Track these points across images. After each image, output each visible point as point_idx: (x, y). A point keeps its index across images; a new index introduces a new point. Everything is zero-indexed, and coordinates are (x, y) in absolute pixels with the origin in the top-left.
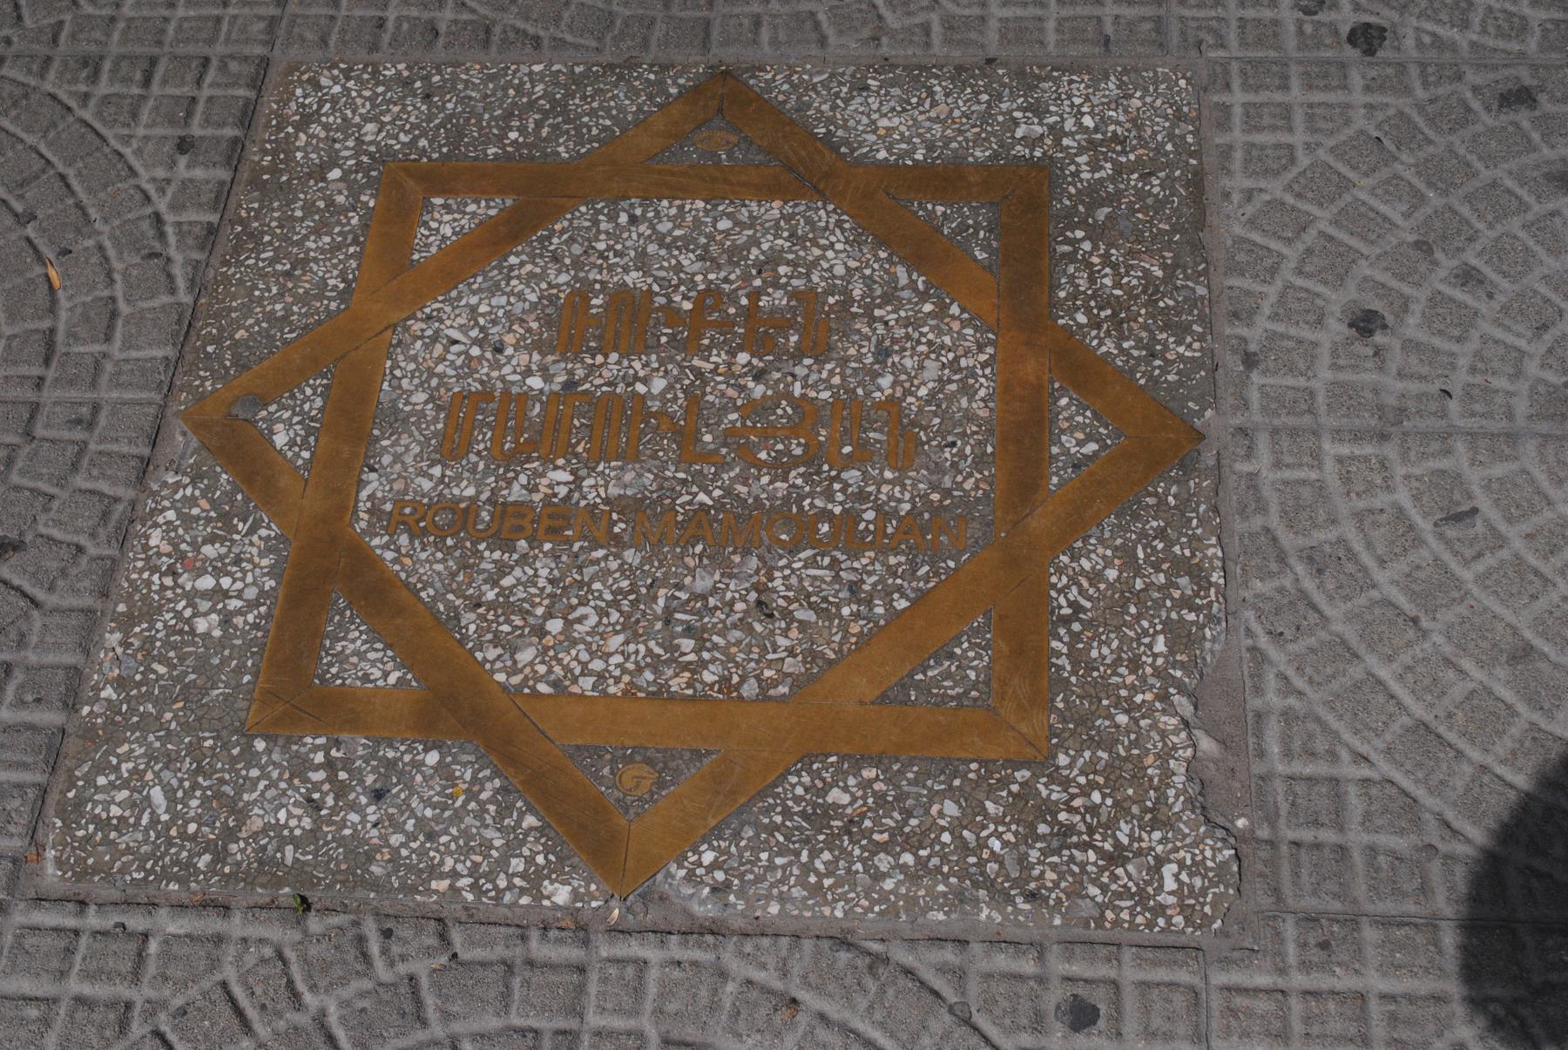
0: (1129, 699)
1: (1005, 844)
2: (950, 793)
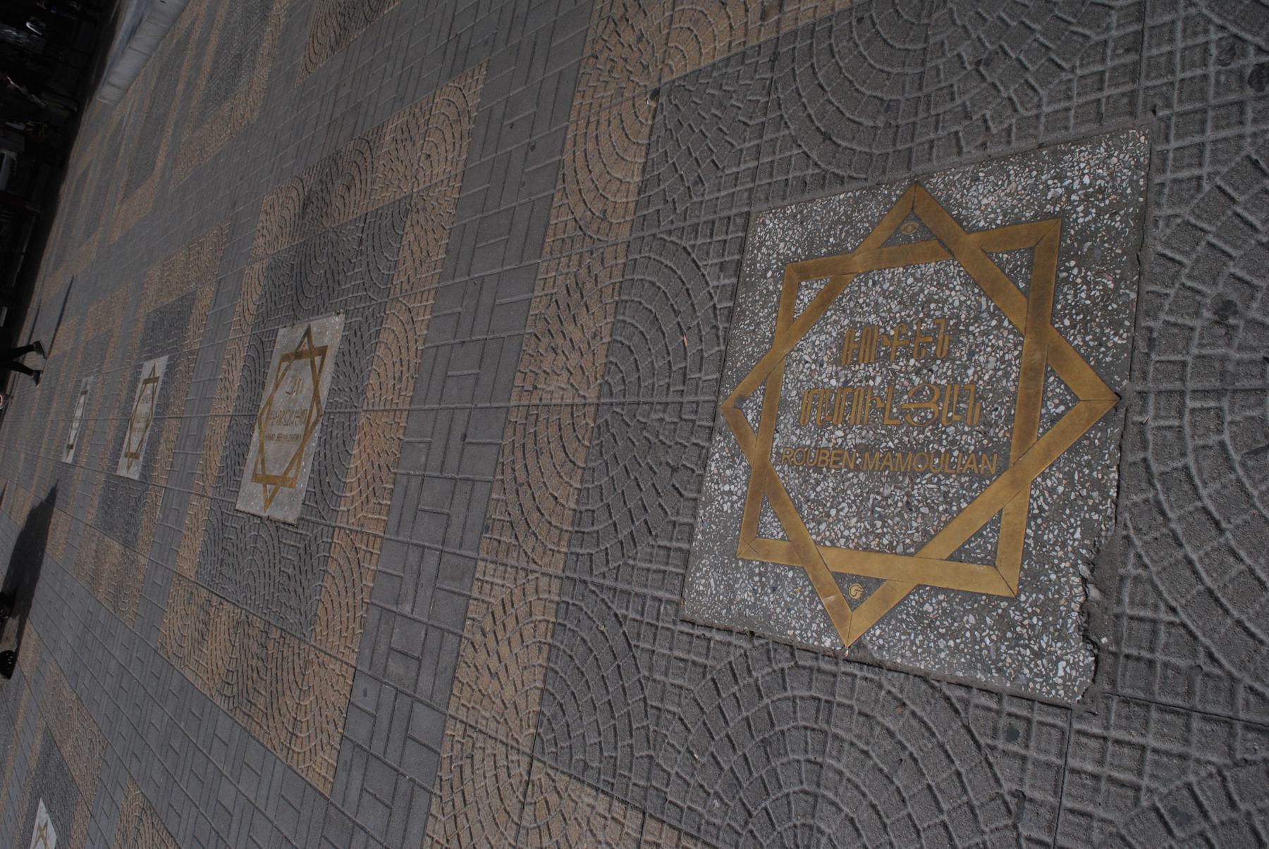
0: (1058, 565)
1: (992, 641)
2: (972, 611)
